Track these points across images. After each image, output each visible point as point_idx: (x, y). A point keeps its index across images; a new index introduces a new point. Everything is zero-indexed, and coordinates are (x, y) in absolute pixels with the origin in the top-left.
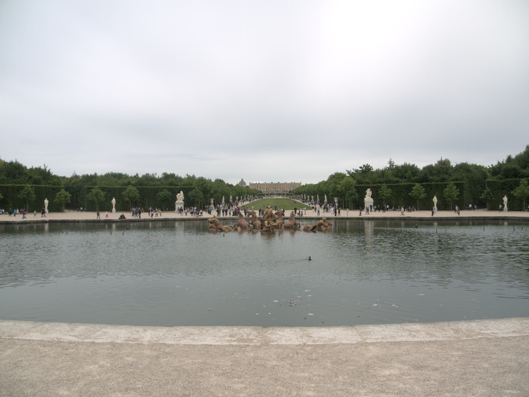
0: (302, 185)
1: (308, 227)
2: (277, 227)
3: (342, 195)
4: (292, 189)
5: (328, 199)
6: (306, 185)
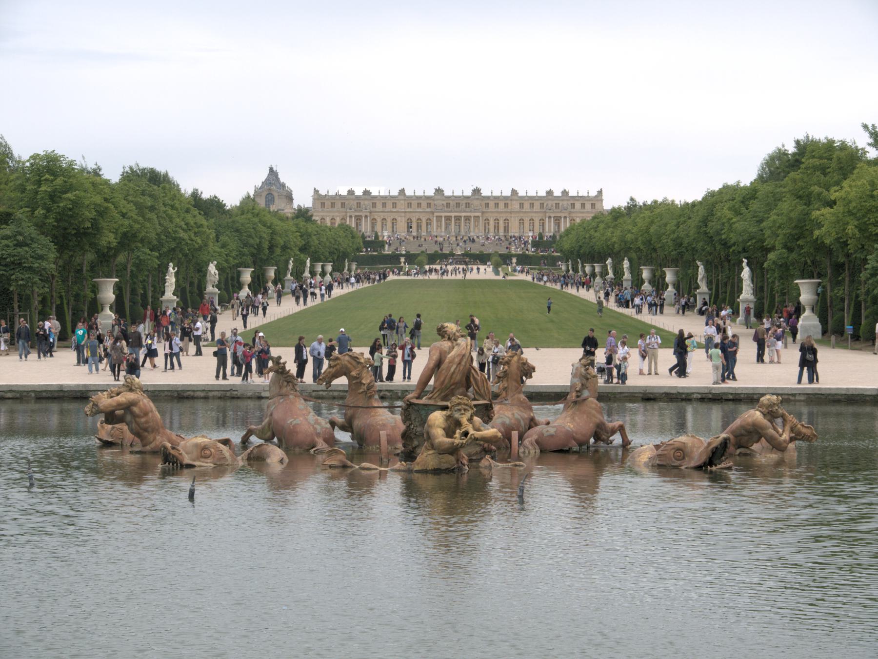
0: (608, 205)
1: (682, 452)
2: (500, 448)
3: (838, 268)
4: (550, 230)
5: (758, 290)
6: (632, 209)
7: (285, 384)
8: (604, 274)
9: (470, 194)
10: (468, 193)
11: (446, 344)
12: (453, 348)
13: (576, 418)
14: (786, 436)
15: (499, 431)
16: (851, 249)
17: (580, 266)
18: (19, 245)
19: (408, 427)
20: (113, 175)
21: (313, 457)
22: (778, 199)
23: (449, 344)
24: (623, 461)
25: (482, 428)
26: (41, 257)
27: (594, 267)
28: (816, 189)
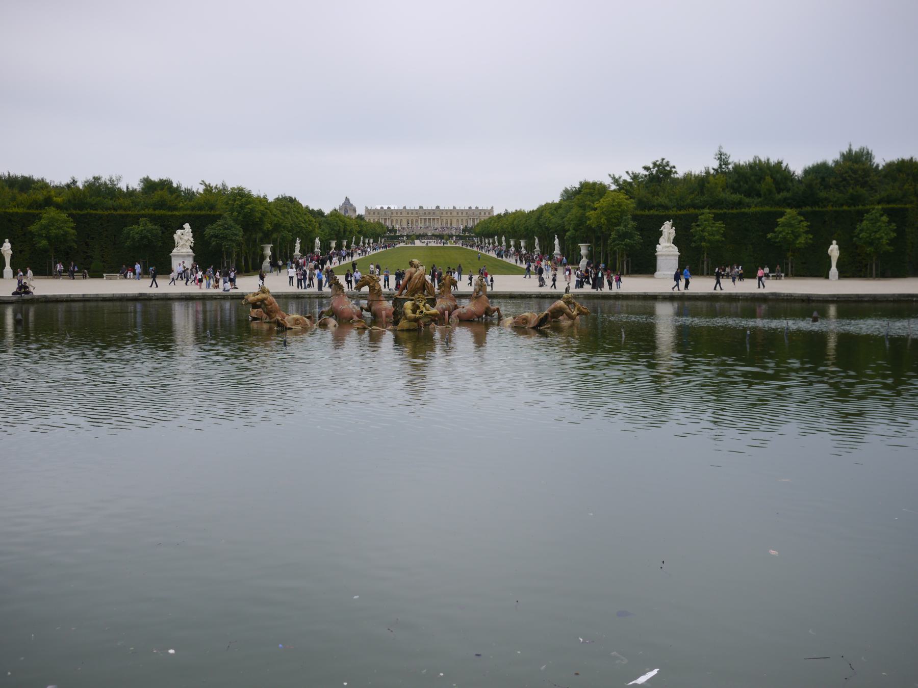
1: (526, 320)
2: (439, 319)
4: (470, 224)
6: (506, 214)
8: (494, 242)
11: (413, 270)
14: (575, 313)
16: (604, 230)
18: (226, 229)
20: (271, 199)
21: (352, 324)
22: (571, 208)
24: (498, 325)
26: (236, 235)
28: (588, 203)
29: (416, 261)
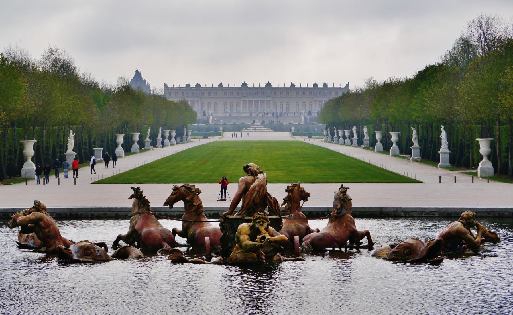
7: (142, 205)
9: (264, 86)
10: (263, 85)
11: (250, 178)
12: (255, 180)
13: (337, 228)
15: (286, 235)
17: (335, 131)
19: (225, 234)
23: (252, 178)
25: (275, 234)
27: (344, 132)
29: (253, 166)
